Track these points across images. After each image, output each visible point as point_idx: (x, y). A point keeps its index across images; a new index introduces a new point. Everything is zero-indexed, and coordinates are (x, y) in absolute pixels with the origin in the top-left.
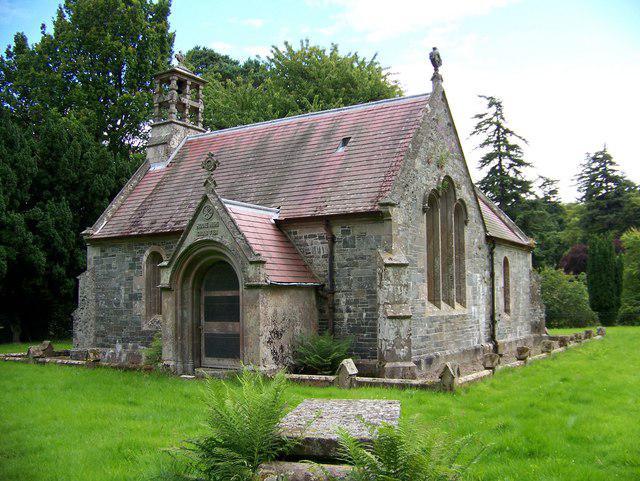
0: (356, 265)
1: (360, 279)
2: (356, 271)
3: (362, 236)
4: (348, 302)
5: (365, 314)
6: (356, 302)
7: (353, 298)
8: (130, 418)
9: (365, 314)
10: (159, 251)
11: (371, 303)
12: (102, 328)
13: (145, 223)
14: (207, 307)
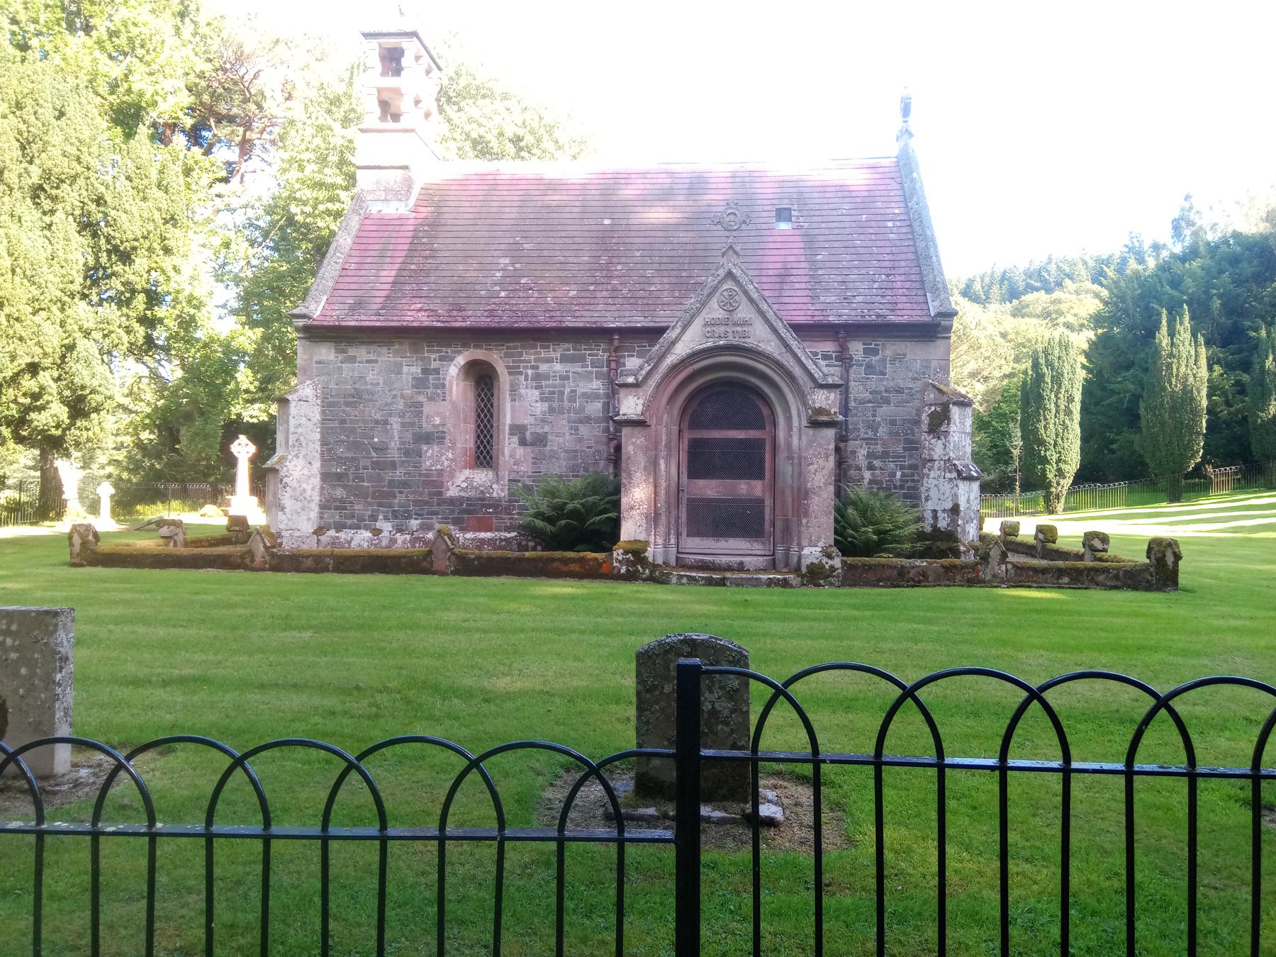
0: (887, 401)
1: (893, 422)
2: (884, 410)
3: (898, 358)
4: (870, 455)
5: (899, 474)
6: (885, 455)
7: (879, 448)
8: (787, 605)
9: (899, 474)
10: (1048, 296)
11: (911, 456)
12: (339, 493)
13: (412, 369)
14: (762, 468)
